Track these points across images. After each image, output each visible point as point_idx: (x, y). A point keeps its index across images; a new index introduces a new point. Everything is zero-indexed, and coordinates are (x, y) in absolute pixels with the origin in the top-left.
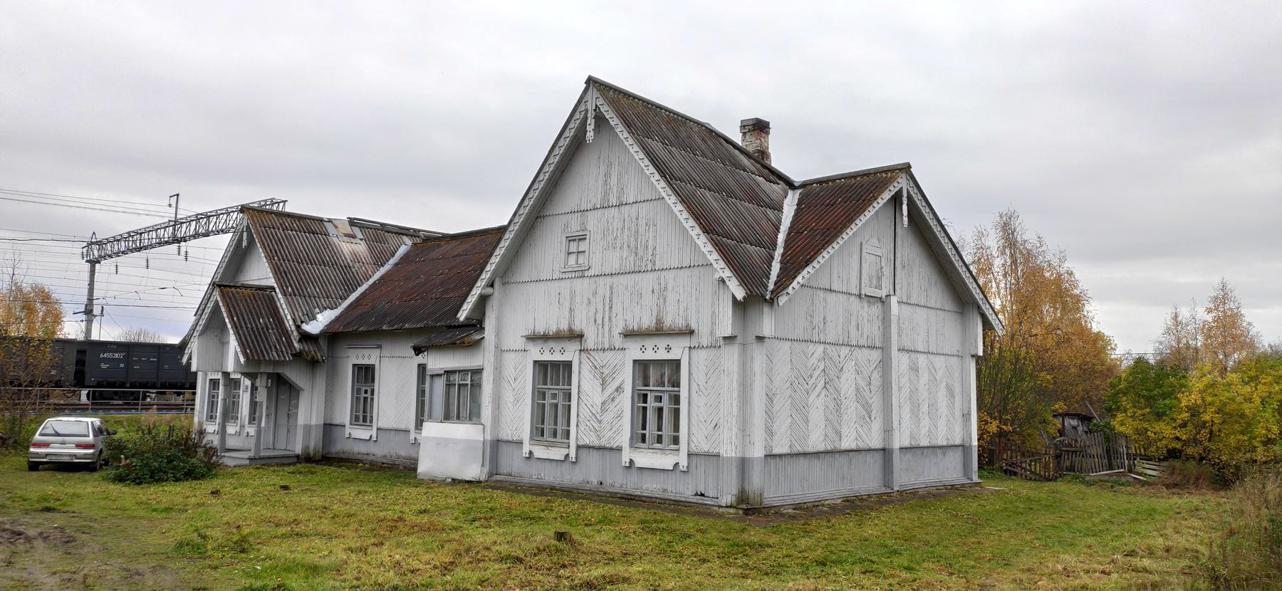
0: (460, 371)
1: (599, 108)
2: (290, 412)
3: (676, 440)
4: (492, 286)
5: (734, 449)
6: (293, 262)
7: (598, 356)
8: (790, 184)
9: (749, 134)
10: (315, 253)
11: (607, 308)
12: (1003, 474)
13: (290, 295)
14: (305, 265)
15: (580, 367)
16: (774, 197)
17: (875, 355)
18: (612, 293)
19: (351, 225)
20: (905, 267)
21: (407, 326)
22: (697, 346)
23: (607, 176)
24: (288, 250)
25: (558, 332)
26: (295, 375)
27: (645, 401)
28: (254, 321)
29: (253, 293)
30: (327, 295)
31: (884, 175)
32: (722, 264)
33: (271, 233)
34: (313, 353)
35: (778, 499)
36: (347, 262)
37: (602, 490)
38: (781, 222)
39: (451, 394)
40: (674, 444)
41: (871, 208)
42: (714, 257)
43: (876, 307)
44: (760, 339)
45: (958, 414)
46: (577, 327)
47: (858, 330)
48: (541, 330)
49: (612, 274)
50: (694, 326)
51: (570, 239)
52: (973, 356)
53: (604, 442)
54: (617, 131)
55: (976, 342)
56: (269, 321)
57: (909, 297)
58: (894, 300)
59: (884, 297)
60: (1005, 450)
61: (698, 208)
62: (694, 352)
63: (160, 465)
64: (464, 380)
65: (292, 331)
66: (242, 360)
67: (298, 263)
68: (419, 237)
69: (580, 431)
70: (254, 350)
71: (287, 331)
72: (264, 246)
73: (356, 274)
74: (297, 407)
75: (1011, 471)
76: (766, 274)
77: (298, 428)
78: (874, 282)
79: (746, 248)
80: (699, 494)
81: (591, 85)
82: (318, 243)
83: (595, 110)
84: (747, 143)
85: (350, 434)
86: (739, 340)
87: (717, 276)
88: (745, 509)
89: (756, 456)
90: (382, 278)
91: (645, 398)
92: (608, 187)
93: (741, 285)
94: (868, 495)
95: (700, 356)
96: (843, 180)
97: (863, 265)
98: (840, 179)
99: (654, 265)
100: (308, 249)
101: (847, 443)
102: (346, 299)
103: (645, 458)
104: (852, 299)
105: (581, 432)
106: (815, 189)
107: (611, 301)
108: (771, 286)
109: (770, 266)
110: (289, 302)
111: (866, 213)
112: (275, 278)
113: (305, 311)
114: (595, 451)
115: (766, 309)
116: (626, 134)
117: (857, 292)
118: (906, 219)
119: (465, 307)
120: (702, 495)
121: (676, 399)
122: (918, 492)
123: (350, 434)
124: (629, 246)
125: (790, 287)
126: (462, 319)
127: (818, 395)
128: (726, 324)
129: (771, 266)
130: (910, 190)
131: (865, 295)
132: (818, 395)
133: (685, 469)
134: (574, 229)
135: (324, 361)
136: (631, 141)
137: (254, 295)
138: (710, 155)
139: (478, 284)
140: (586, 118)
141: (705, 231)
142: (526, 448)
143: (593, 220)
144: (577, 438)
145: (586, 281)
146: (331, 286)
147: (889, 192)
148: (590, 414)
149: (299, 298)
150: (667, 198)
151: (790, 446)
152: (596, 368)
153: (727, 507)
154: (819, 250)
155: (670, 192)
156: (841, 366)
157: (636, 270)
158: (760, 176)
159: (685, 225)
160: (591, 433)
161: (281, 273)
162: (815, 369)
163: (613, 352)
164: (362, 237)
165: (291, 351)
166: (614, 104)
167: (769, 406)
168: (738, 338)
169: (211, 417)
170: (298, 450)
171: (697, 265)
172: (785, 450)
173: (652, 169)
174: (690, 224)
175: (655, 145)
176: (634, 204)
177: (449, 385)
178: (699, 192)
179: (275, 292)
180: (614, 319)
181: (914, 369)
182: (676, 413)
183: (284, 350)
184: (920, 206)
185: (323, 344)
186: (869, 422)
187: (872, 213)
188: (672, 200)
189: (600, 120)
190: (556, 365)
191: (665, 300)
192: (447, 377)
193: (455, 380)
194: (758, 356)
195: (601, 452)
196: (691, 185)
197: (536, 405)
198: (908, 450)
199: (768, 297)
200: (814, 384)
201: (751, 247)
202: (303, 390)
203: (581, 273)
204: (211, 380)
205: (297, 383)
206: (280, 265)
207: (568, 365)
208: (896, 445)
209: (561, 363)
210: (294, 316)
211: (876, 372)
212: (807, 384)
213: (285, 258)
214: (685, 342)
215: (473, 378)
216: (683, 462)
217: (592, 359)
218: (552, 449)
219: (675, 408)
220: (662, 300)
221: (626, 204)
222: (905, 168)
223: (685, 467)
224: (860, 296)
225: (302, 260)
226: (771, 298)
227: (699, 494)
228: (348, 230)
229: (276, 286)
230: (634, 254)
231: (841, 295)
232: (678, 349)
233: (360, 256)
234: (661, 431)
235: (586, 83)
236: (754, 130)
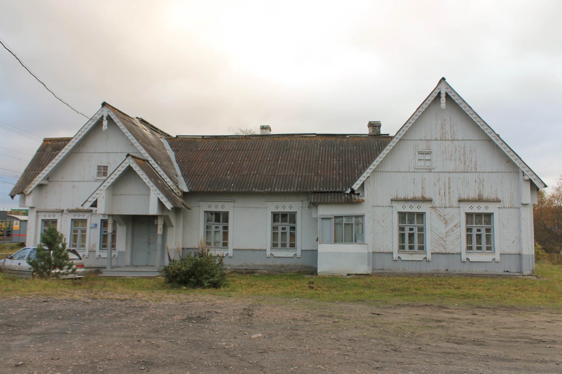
7: (442, 211)
11: (447, 188)
18: (450, 181)
22: (503, 207)
46: (427, 196)
48: (402, 196)
99: (476, 169)
114: (442, 255)
120: (507, 271)
134: (422, 146)
148: (439, 238)
152: (441, 216)
153: (528, 275)
157: (465, 171)
160: (440, 247)
180: (452, 193)
192: (335, 219)
203: (430, 170)
209: (288, 213)
214: (497, 205)
216: (498, 258)
218: (414, 255)
220: (481, 186)
230: (463, 164)
232: (423, 208)
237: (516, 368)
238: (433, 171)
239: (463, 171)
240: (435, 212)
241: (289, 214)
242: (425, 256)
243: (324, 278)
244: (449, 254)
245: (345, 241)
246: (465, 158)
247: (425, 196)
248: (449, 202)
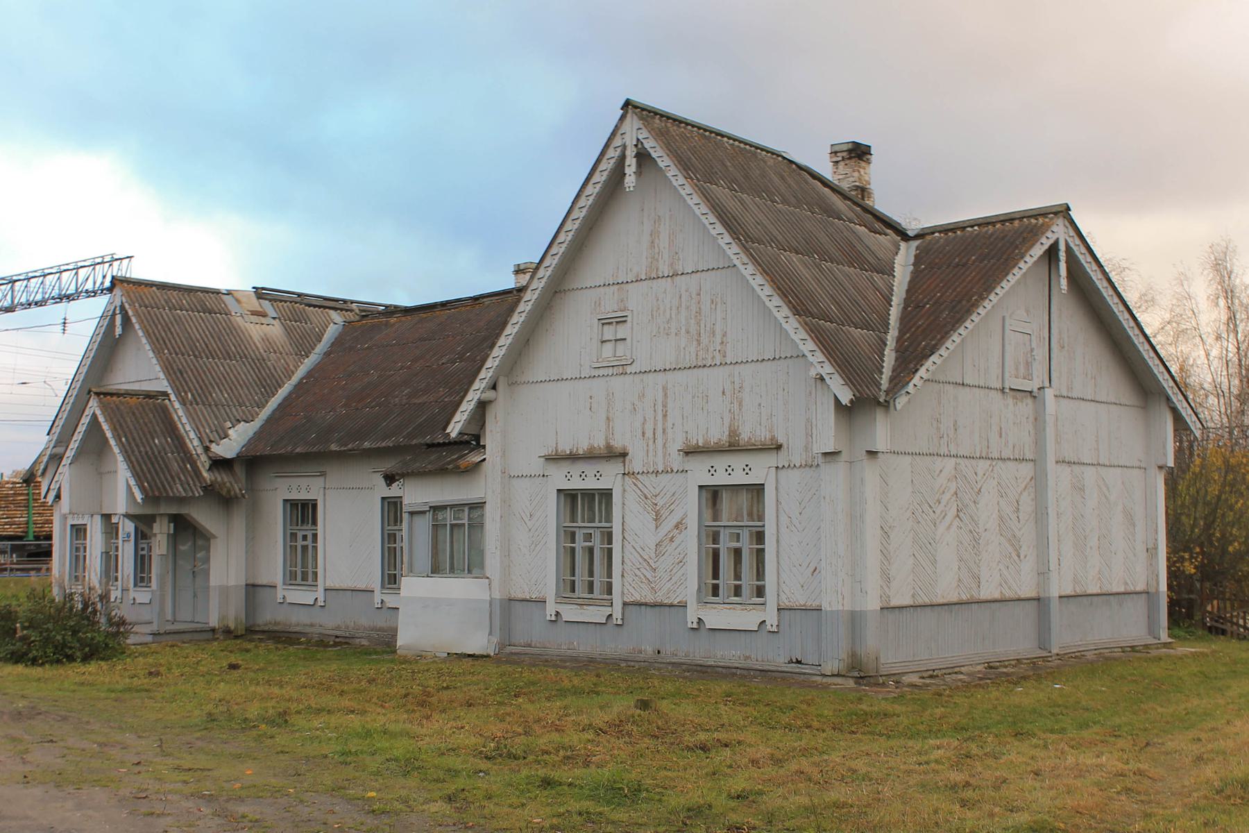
0: (452, 506)
1: (642, 143)
2: (196, 569)
3: (760, 592)
4: (494, 387)
5: (840, 600)
6: (189, 356)
8: (905, 236)
9: (842, 163)
10: (215, 342)
11: (660, 417)
12: (1206, 632)
13: (191, 404)
14: (205, 359)
15: (623, 497)
16: (881, 255)
17: (1026, 470)
18: (666, 395)
19: (259, 298)
20: (1063, 347)
21: (367, 445)
22: (786, 466)
23: (654, 234)
24: (180, 339)
25: (592, 449)
26: (204, 517)
27: (573, 541)
28: (149, 443)
29: (140, 403)
30: (239, 402)
31: (1033, 221)
32: (820, 356)
33: (156, 315)
34: (228, 484)
35: (897, 665)
36: (260, 353)
37: (660, 660)
38: (893, 290)
39: (440, 538)
40: (757, 597)
41: (1015, 271)
42: (808, 346)
43: (1024, 404)
44: (872, 454)
45: (1140, 548)
46: (618, 444)
47: (1001, 437)
49: (665, 370)
50: (781, 441)
51: (605, 322)
52: (1160, 468)
53: (660, 597)
54: (669, 174)
55: (1164, 447)
56: (167, 441)
57: (1070, 388)
58: (1049, 394)
59: (1035, 390)
60: (1210, 599)
61: (784, 281)
62: (782, 473)
63: (63, 639)
64: (459, 519)
65: (197, 455)
66: (139, 496)
67: (195, 356)
68: (351, 311)
69: (626, 584)
70: (153, 484)
71: (191, 455)
72: (149, 335)
73: (273, 370)
74: (207, 560)
75: (1217, 628)
76: (877, 368)
77: (212, 593)
78: (1022, 370)
79: (849, 332)
80: (794, 660)
81: (630, 111)
82: (218, 326)
83: (636, 146)
84: (841, 177)
85: (284, 598)
86: (844, 457)
87: (813, 373)
88: (857, 677)
89: (870, 608)
90: (310, 374)
91: (715, 538)
92: (657, 250)
93: (847, 384)
94: (1017, 660)
95: (792, 479)
96: (976, 228)
97: (1007, 347)
98: (972, 227)
99: (724, 356)
100: (206, 336)
101: (988, 591)
102: (264, 406)
103: (718, 617)
104: (993, 394)
105: (627, 585)
106: (938, 241)
107: (665, 406)
108: (885, 382)
109: (882, 355)
110: (191, 414)
111: (1010, 277)
112: (168, 380)
113: (212, 425)
114: (648, 608)
115: (880, 415)
116: (681, 180)
117: (999, 386)
118: (1064, 282)
119: (457, 417)
120: (799, 662)
121: (760, 537)
122: (1083, 656)
123: (284, 598)
124: (688, 332)
125: (911, 384)
126: (453, 435)
127: (949, 528)
128: (827, 434)
129: (883, 355)
130: (1070, 240)
131: (1011, 389)
132: (949, 528)
133: (620, 622)
134: (610, 307)
135: (243, 496)
136: (689, 189)
137: (142, 406)
138: (793, 200)
139: (476, 385)
140: (623, 158)
141: (796, 312)
142: (551, 609)
143: (637, 299)
144: (623, 593)
145: (628, 379)
146: (242, 389)
147: (1040, 246)
148: (641, 560)
149: (203, 408)
150: (741, 268)
151: (913, 596)
152: (646, 498)
153: (833, 675)
154: (947, 333)
155: (746, 260)
156: (979, 487)
157: (699, 364)
158: (861, 225)
159: (768, 303)
161: (175, 373)
162: (944, 492)
163: (669, 475)
164: (275, 316)
165: (200, 483)
166: (662, 136)
167: (884, 543)
168: (843, 454)
169: (142, 579)
170: (214, 622)
171: (783, 357)
172: (907, 601)
173: (720, 228)
174: (775, 302)
175: (721, 192)
176: (694, 274)
177: (436, 527)
178: (785, 256)
179: (170, 400)
180: (669, 431)
181: (1079, 488)
182: (760, 553)
183: (191, 482)
184: (1083, 262)
185: (240, 471)
186: (1018, 561)
187: (1018, 276)
188: (748, 270)
189: (643, 157)
190: (589, 495)
191: (740, 405)
192: (433, 515)
193: (445, 519)
194: (870, 473)
195: (657, 609)
196: (773, 248)
197: (562, 550)
198: (1071, 599)
199: (881, 400)
200: (942, 511)
201: (856, 331)
202: (215, 537)
203: (621, 368)
204: (72, 526)
205: (203, 523)
206: (172, 362)
207: (607, 495)
208: (1055, 592)
209: (579, 492)
210: (200, 433)
211: (1025, 494)
212: (934, 512)
213: (177, 350)
214: (771, 460)
215: (471, 516)
216: (772, 619)
217: (640, 485)
219: (608, 548)
220: (736, 405)
221: (682, 274)
222: (1062, 212)
223: (774, 626)
224: (1003, 390)
225: (200, 353)
226: (886, 401)
227: (794, 660)
228: (255, 304)
229: (170, 391)
231: (977, 390)
232: (759, 470)
233: (276, 344)
234: (740, 579)
235: (622, 109)
236: (850, 158)
238: (629, 369)
239: (695, 364)
240: (635, 488)
241: (302, 504)
243: (405, 661)
244: (662, 605)
245: (452, 569)
246: (698, 324)
247: (612, 443)
248: (664, 457)
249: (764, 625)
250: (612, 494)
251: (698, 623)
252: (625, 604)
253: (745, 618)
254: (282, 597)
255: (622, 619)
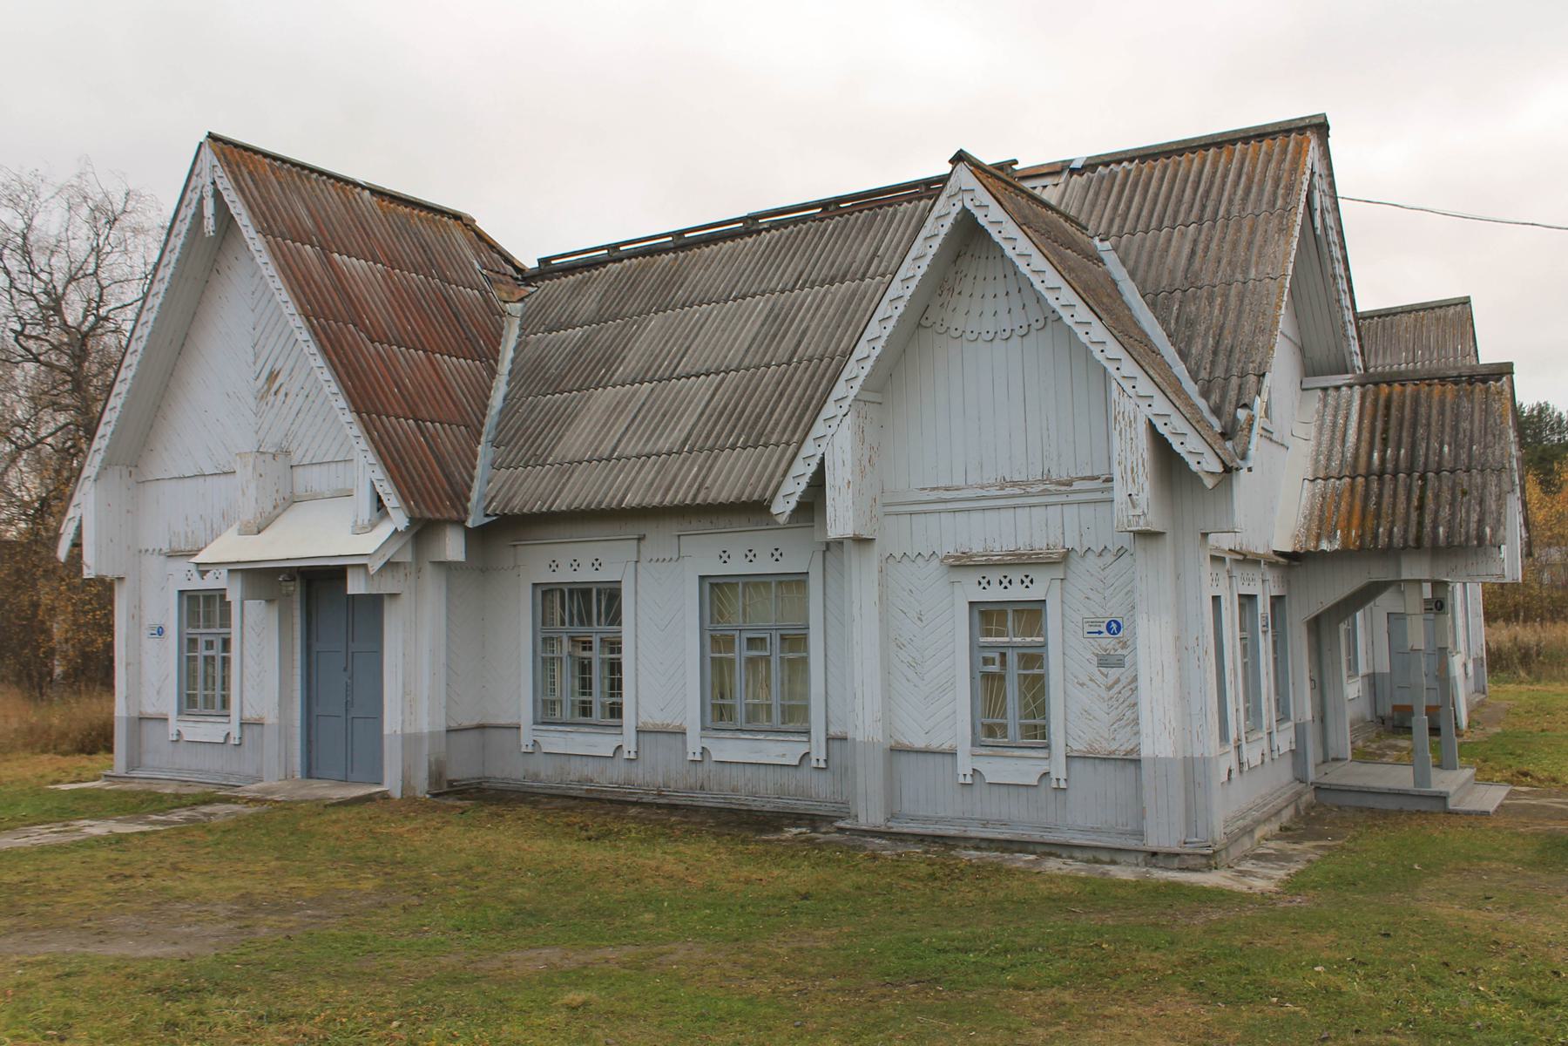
3: (616, 711)
133: (632, 756)
190: (582, 593)
209: (201, 594)
237: (284, 1019)
241: (204, 596)
242: (1044, 767)
249: (806, 757)
250: (620, 590)
251: (702, 753)
252: (639, 732)
253: (602, 744)
254: (175, 732)
255: (636, 752)
